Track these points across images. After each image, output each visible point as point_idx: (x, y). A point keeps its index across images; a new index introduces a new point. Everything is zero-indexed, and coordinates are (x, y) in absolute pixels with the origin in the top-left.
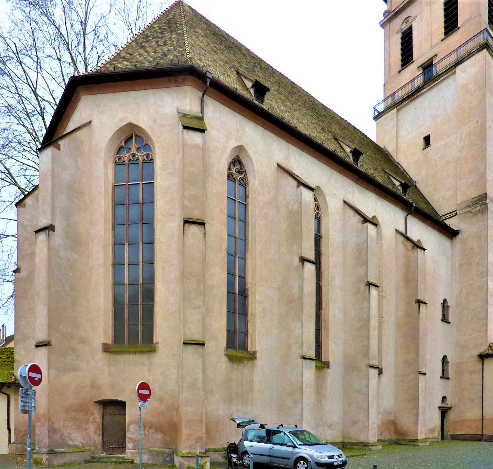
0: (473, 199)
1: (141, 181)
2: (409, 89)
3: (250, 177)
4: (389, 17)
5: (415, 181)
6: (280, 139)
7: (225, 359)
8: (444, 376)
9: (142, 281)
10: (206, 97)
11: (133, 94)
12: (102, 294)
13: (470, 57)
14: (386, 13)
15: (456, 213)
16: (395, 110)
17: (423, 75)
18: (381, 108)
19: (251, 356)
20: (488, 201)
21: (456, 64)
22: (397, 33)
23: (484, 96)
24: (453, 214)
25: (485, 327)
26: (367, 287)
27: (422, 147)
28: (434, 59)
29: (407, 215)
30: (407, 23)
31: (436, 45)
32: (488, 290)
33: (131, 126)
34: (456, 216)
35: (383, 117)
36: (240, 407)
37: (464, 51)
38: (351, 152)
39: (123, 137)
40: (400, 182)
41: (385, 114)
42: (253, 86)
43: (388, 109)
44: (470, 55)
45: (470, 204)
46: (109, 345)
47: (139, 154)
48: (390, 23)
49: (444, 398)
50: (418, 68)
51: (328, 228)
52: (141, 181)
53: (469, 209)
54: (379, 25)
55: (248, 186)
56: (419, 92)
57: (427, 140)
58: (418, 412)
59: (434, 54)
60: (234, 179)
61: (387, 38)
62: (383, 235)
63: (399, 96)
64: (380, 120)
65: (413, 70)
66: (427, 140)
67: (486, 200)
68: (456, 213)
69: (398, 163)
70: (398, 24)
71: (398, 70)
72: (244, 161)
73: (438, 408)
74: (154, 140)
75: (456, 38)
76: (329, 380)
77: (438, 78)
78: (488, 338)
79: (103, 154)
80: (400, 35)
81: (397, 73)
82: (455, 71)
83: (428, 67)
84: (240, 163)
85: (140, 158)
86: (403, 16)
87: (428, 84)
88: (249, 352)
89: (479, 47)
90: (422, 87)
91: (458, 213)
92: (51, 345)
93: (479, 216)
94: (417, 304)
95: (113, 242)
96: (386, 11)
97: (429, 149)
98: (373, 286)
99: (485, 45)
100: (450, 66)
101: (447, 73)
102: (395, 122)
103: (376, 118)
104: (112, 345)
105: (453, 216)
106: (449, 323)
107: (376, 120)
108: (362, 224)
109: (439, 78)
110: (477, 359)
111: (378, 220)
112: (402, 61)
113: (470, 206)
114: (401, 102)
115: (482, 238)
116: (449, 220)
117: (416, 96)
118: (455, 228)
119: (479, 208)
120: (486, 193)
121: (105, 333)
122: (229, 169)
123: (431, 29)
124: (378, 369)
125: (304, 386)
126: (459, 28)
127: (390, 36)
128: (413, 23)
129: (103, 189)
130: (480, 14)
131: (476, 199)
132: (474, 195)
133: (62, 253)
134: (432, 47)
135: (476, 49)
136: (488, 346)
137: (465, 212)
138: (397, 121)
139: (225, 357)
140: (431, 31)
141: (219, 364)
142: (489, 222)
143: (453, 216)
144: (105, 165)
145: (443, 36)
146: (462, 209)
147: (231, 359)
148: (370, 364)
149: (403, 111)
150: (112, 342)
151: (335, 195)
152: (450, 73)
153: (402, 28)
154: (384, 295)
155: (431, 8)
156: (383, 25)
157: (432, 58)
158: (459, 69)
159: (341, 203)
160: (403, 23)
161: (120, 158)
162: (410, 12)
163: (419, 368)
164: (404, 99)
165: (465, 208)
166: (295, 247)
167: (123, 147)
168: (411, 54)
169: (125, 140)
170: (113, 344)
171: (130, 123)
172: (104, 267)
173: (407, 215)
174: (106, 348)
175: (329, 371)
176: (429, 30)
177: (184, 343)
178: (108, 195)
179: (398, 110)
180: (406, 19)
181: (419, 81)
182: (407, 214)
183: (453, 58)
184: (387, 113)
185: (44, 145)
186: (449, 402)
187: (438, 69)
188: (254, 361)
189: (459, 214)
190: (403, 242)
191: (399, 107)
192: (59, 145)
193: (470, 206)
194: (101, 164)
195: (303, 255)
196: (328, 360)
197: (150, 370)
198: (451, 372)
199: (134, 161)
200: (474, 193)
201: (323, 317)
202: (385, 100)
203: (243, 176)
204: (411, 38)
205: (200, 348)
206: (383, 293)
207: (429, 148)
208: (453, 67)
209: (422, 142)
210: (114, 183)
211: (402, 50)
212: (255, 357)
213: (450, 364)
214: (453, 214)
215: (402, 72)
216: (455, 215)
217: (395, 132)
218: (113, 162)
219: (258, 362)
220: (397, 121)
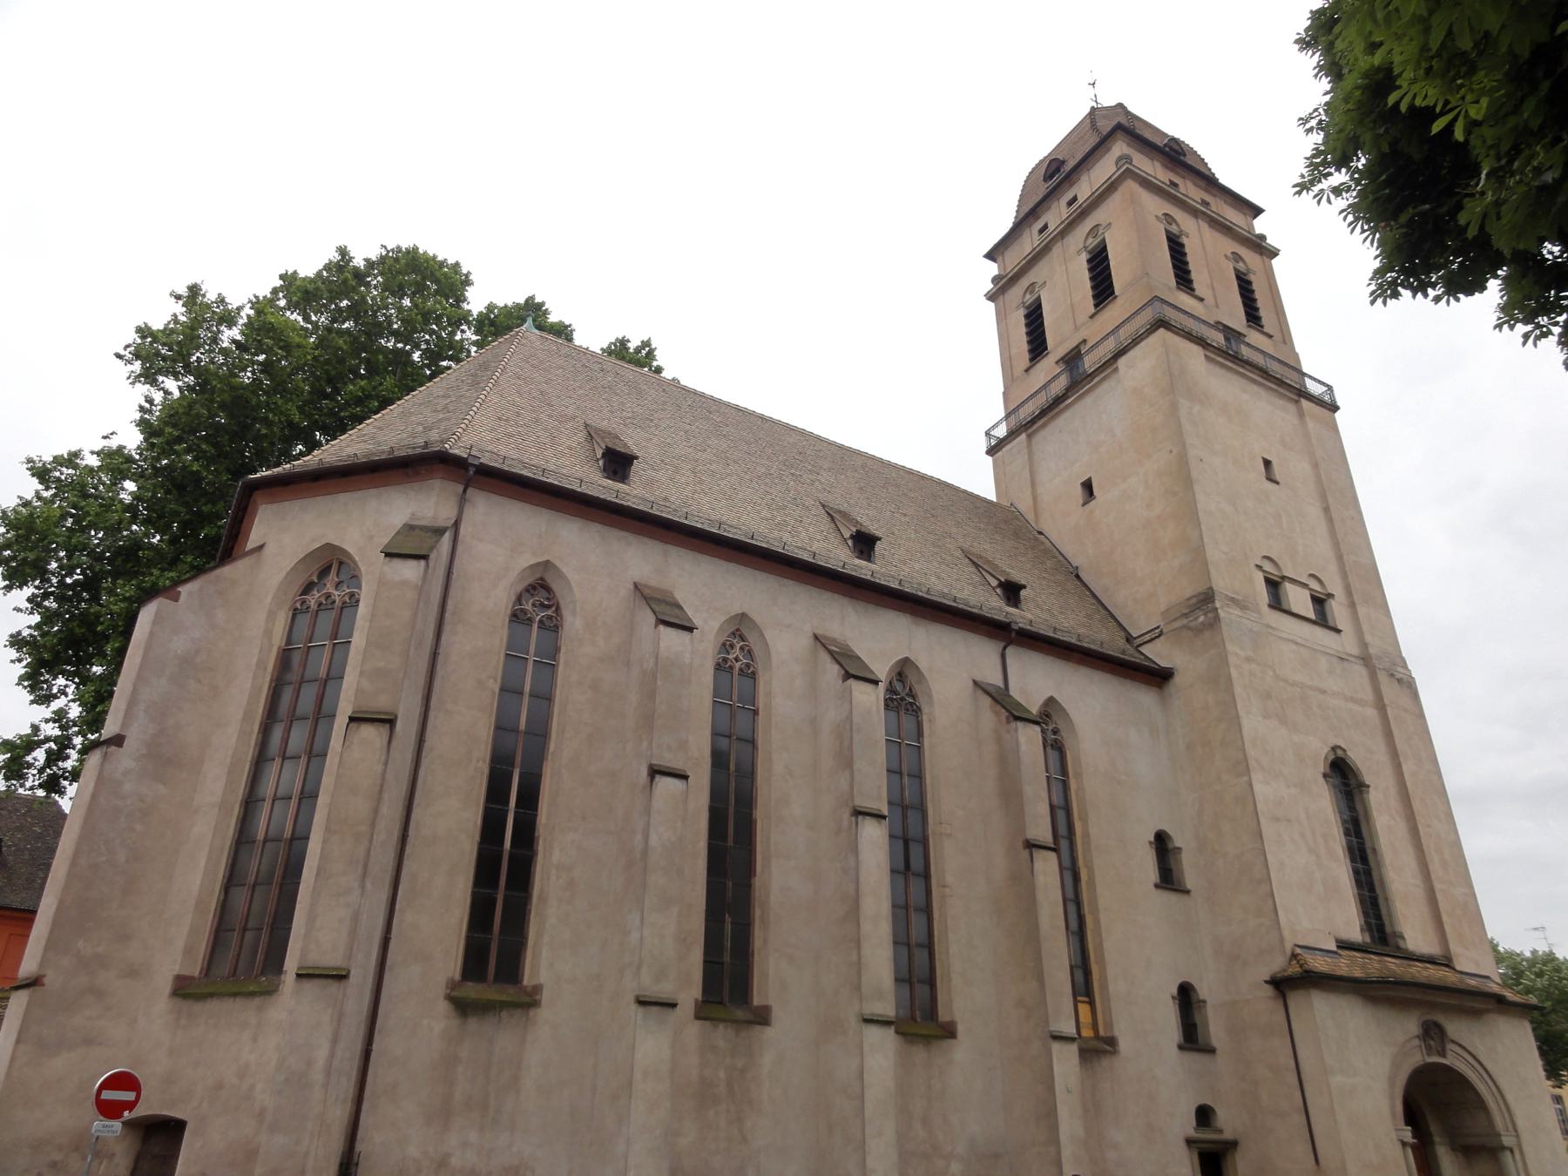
0: (1188, 599)
1: (331, 639)
2: (1042, 400)
3: (566, 613)
4: (1000, 285)
5: (1077, 567)
6: (646, 540)
7: (443, 1006)
8: (1192, 1038)
9: (290, 833)
10: (470, 491)
11: (343, 497)
12: (202, 863)
13: (1138, 343)
14: (995, 280)
15: (1161, 631)
16: (1023, 436)
17: (1068, 373)
18: (1001, 432)
19: (528, 999)
20: (1218, 604)
21: (1115, 355)
22: (1017, 308)
23: (1174, 407)
24: (1156, 634)
25: (1270, 903)
26: (853, 819)
27: (1081, 502)
28: (1082, 347)
29: (1005, 648)
30: (1031, 293)
31: (1083, 324)
32: (1259, 806)
33: (329, 548)
34: (1161, 638)
35: (1004, 449)
36: (473, 1136)
37: (1125, 334)
38: (852, 537)
39: (316, 567)
40: (998, 579)
41: (1007, 443)
42: (604, 455)
43: (1012, 434)
44: (1136, 341)
45: (1185, 611)
46: (192, 978)
47: (337, 593)
48: (1003, 294)
49: (1204, 1115)
50: (1057, 363)
51: (770, 693)
52: (331, 639)
53: (1185, 621)
54: (984, 298)
55: (562, 628)
56: (1060, 403)
57: (1088, 487)
58: (1059, 1153)
59: (1081, 340)
60: (529, 619)
61: (1001, 317)
62: (935, 695)
63: (1031, 409)
64: (1000, 454)
65: (1048, 366)
66: (1088, 487)
67: (1213, 601)
68: (1161, 631)
69: (1040, 533)
70: (1016, 293)
71: (1025, 368)
72: (554, 586)
73: (1183, 1145)
74: (363, 569)
75: (1114, 313)
76: (767, 1059)
77: (1089, 378)
78: (1286, 934)
79: (269, 599)
80: (1022, 312)
81: (1054, 364)
82: (1117, 368)
83: (1072, 359)
84: (547, 588)
85: (337, 599)
86: (1025, 282)
87: (1075, 390)
88: (526, 987)
89: (1149, 327)
90: (1064, 394)
91: (1164, 631)
92: (43, 985)
93: (1207, 634)
94: (1027, 851)
95: (552, 703)
96: (996, 276)
97: (1093, 503)
98: (868, 818)
99: (1159, 323)
100: (1106, 359)
101: (1104, 370)
102: (1026, 457)
103: (991, 451)
104: (200, 978)
105: (1156, 637)
106: (1188, 892)
107: (992, 456)
108: (843, 682)
109: (1092, 380)
110: (1269, 991)
111: (917, 667)
112: (1030, 351)
113: (1185, 615)
114: (1033, 421)
115: (1219, 679)
116: (1149, 645)
117: (1057, 410)
118: (1164, 664)
119: (1202, 619)
120: (1211, 588)
121: (188, 951)
122: (519, 599)
123: (1071, 300)
124: (893, 1027)
125: (638, 1075)
126: (1116, 297)
127: (1005, 315)
128: (1041, 293)
129: (255, 660)
130: (1147, 274)
131: (1194, 601)
132: (1189, 592)
133: (128, 787)
134: (1077, 328)
135: (1144, 330)
136: (1289, 952)
137: (1174, 630)
138: (1030, 453)
139: (446, 1002)
140: (1072, 305)
141: (425, 1022)
142: (1230, 647)
143: (1156, 637)
144: (271, 616)
145: (1092, 310)
146: (1171, 621)
147: (463, 1007)
148: (864, 1012)
149: (1038, 438)
150: (200, 973)
151: (789, 626)
152: (1109, 371)
153: (1025, 300)
154: (949, 831)
155: (1066, 269)
156: (991, 297)
157: (1078, 346)
158: (1122, 362)
159: (805, 642)
160: (1025, 292)
161: (303, 602)
162: (1036, 275)
163: (1047, 1022)
164: (1035, 417)
165: (1175, 620)
166: (645, 744)
167: (314, 582)
168: (1044, 341)
169: (319, 570)
170: (202, 975)
171: (328, 543)
172: (220, 809)
173: (1005, 648)
174: (183, 989)
175: (769, 1032)
176: (1069, 302)
177: (299, 975)
178: (265, 669)
179: (1029, 437)
180: (1028, 287)
181: (1063, 382)
182: (1004, 643)
183: (1110, 346)
184: (1010, 442)
185: (1040, 330)
186: (1228, 1122)
187: (1089, 363)
188: (532, 1013)
189: (1167, 633)
190: (991, 707)
191: (1030, 431)
192: (180, 592)
193: (1185, 615)
194: (261, 616)
195: (654, 762)
196: (765, 1003)
197: (255, 1040)
198: (1215, 1028)
199: (326, 604)
200: (1188, 589)
201: (757, 894)
202: (1008, 416)
203: (549, 612)
204: (1041, 315)
205: (333, 987)
206: (943, 825)
207: (1093, 502)
208: (1111, 361)
209: (1078, 491)
210: (283, 644)
211: (1028, 334)
212: (535, 1000)
213: (1209, 1006)
214: (1156, 634)
215: (1032, 371)
216: (1160, 636)
217: (1028, 475)
218: (289, 610)
219: (543, 1014)
220: (1030, 453)
